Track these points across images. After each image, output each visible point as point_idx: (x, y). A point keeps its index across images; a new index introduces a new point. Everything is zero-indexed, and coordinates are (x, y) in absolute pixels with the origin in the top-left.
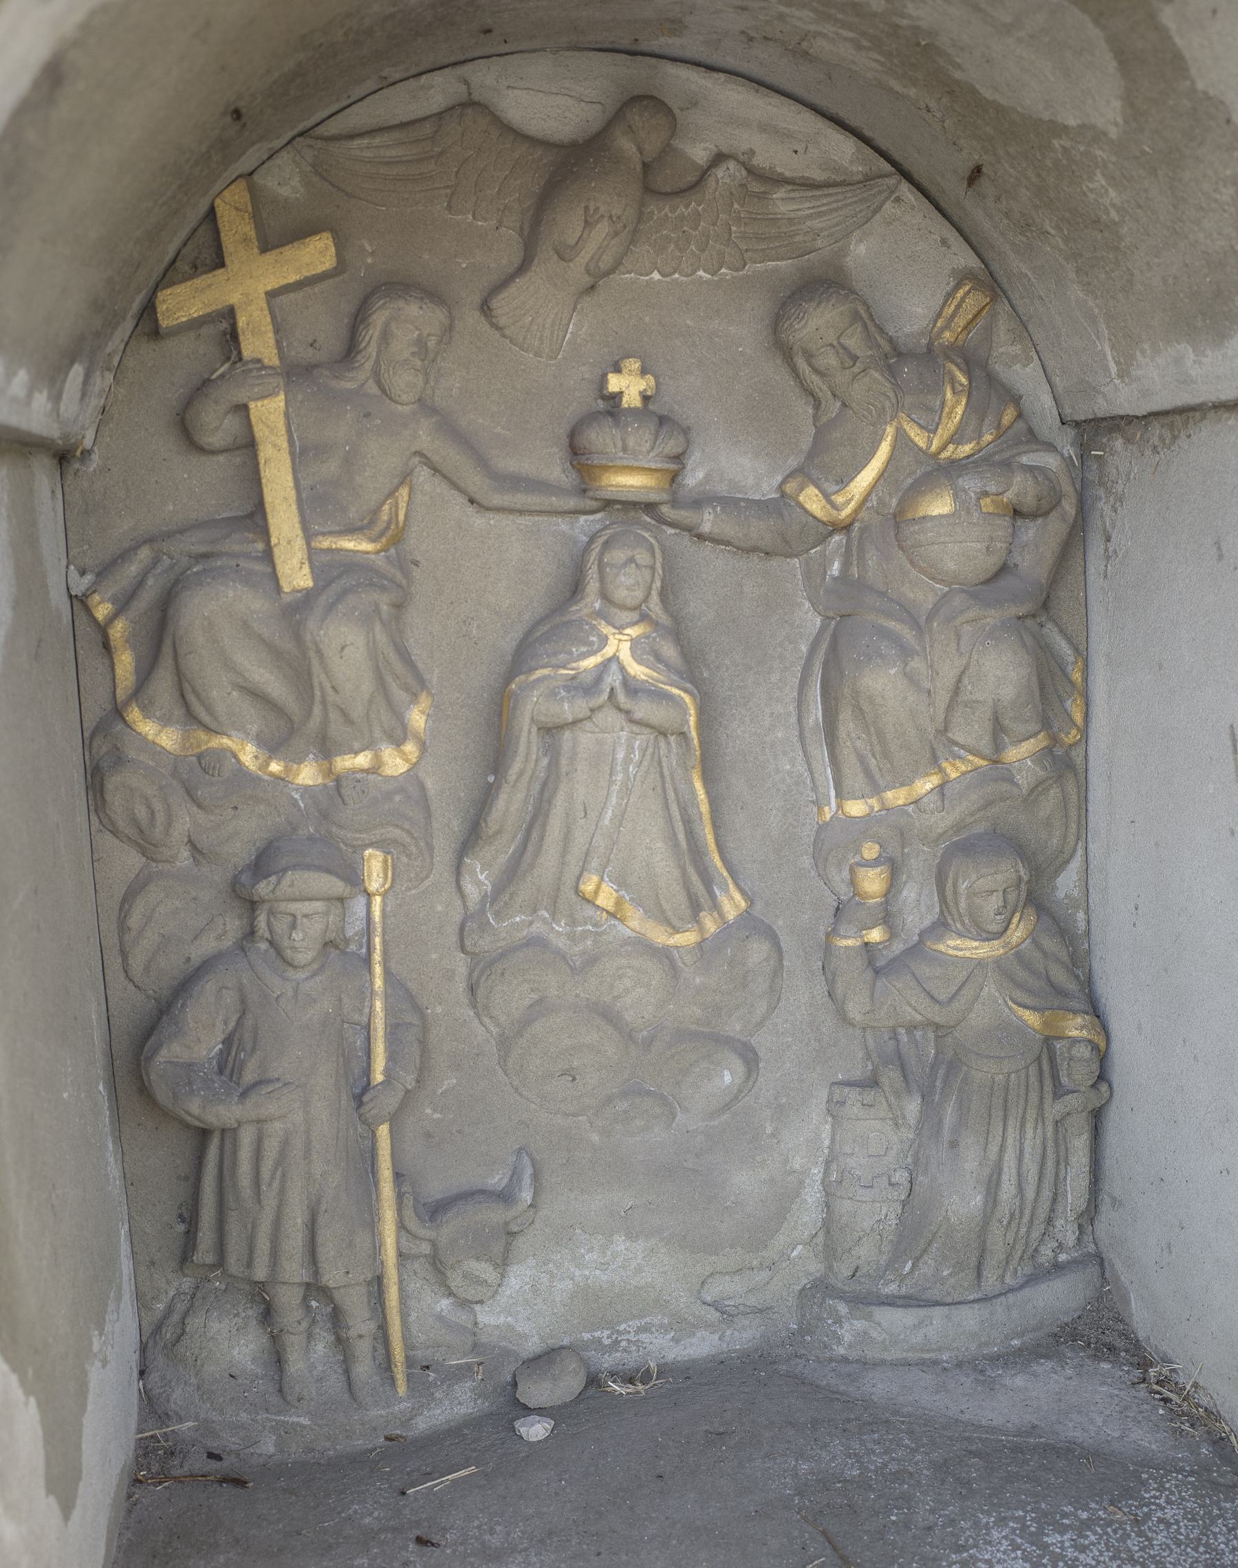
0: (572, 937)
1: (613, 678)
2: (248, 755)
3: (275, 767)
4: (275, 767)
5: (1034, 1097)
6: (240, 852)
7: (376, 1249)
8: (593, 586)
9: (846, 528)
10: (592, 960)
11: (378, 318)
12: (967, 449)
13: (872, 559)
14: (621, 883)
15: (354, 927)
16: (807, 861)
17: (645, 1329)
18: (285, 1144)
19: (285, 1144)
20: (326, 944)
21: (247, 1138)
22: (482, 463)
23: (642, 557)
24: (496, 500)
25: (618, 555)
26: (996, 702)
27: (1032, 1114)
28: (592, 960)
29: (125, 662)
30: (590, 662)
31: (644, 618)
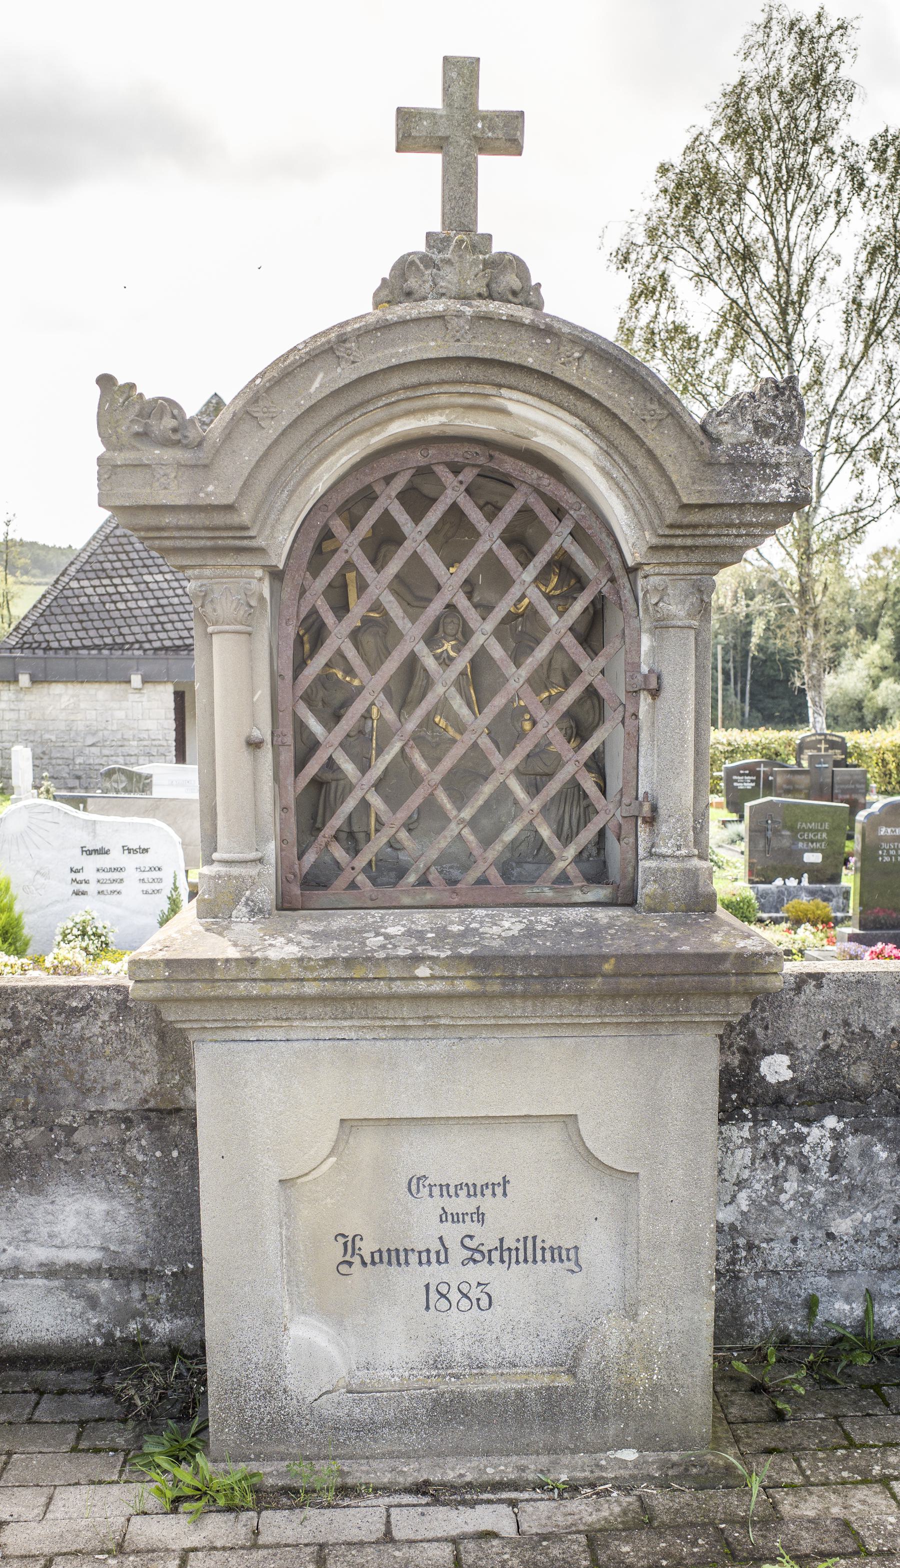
0: (433, 737)
1: (445, 655)
2: (340, 675)
3: (348, 679)
4: (348, 679)
5: (576, 797)
6: (336, 702)
7: (368, 825)
8: (441, 629)
9: (522, 615)
10: (438, 744)
11: (383, 550)
12: (558, 592)
13: (528, 624)
14: (447, 719)
15: (368, 730)
16: (509, 721)
17: (451, 867)
18: (344, 788)
19: (344, 788)
20: (417, 473)
21: (333, 785)
22: (412, 592)
23: (455, 621)
24: (415, 604)
25: (449, 620)
26: (562, 670)
27: (575, 803)
28: (438, 744)
29: (307, 647)
30: (439, 651)
31: (456, 639)
